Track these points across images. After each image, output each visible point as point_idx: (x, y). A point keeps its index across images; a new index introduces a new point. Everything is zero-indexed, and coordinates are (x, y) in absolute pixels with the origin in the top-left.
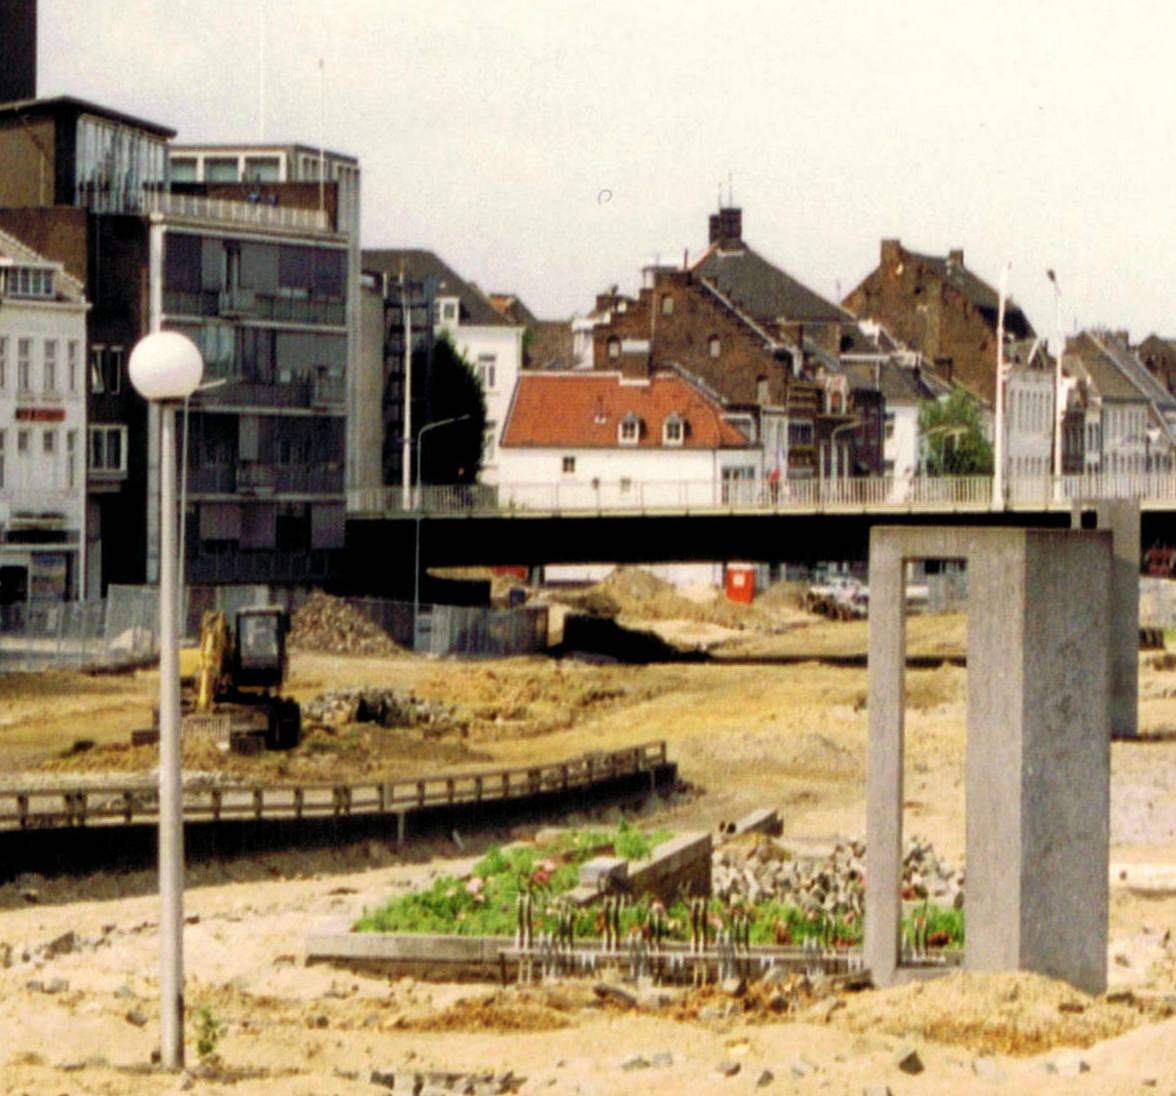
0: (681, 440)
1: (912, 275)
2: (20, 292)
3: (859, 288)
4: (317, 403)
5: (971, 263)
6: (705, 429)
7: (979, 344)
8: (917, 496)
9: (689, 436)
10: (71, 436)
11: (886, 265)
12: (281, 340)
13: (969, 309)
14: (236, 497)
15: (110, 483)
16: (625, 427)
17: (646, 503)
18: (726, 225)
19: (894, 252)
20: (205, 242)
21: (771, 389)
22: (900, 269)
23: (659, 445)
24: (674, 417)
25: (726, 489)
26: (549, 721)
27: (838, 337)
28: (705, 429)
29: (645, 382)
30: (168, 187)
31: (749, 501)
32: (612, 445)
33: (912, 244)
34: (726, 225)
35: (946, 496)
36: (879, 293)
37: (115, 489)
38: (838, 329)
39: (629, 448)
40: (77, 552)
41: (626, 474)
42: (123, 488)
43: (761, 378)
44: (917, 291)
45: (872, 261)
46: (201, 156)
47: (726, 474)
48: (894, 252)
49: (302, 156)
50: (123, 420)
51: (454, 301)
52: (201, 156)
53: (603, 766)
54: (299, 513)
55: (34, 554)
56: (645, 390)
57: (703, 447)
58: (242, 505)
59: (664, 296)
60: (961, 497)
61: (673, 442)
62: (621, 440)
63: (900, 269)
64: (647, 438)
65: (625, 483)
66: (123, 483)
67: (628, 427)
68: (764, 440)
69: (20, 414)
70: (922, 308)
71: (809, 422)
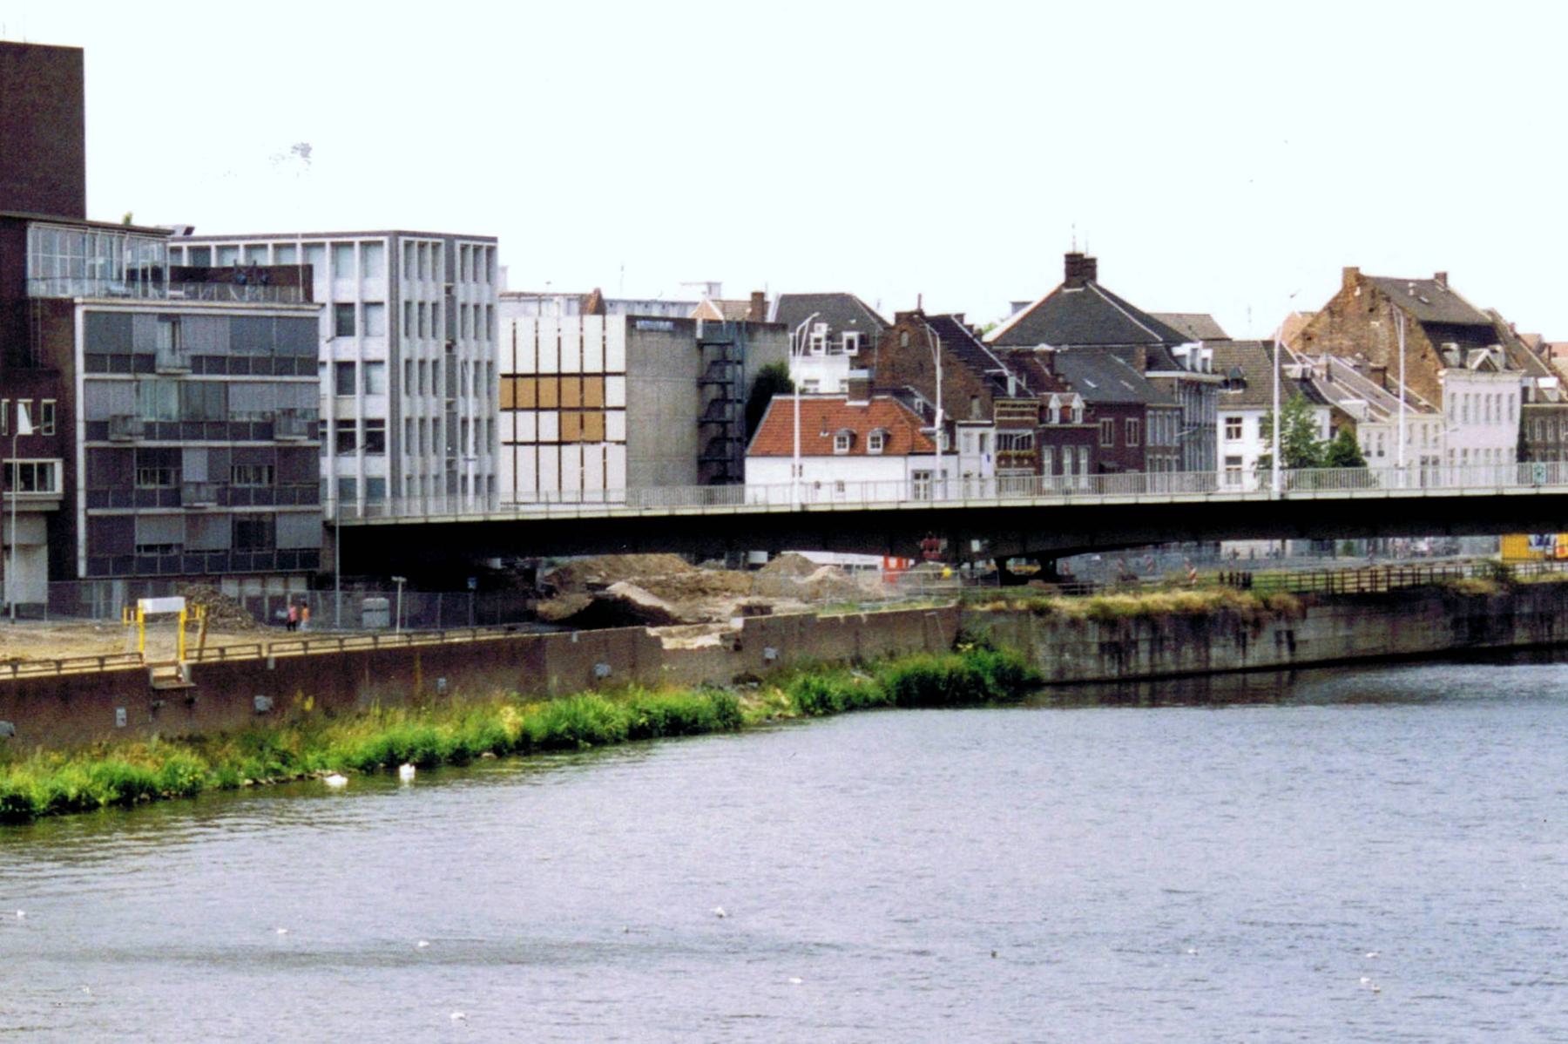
1: (1367, 297)
3: (1325, 309)
5: (1454, 284)
6: (900, 442)
7: (1421, 353)
8: (1291, 484)
9: (889, 445)
11: (1347, 290)
12: (232, 389)
15: (50, 501)
16: (839, 439)
17: (772, 501)
18: (1080, 268)
19: (1354, 278)
20: (135, 320)
21: (982, 405)
22: (1358, 293)
23: (864, 454)
24: (877, 432)
26: (1089, 675)
29: (865, 403)
30: (167, 275)
31: (948, 496)
32: (829, 453)
33: (1367, 271)
34: (1080, 268)
35: (695, 501)
36: (1341, 313)
37: (56, 507)
38: (1144, 351)
41: (841, 478)
43: (974, 397)
44: (1371, 310)
45: (1334, 287)
46: (299, 242)
47: (917, 476)
48: (1354, 278)
50: (56, 455)
51: (854, 335)
52: (242, 243)
54: (266, 519)
56: (864, 410)
57: (898, 454)
58: (188, 516)
59: (902, 331)
60: (711, 500)
61: (876, 451)
62: (837, 450)
63: (1358, 293)
64: (855, 447)
65: (841, 486)
66: (61, 502)
67: (841, 439)
70: (1375, 324)
71: (1030, 432)
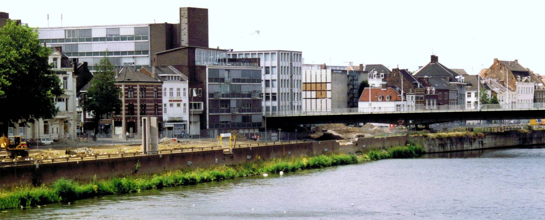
0: (381, 100)
1: (499, 65)
2: (174, 80)
4: (215, 97)
5: (519, 62)
8: (482, 108)
9: (391, 99)
10: (185, 105)
11: (495, 64)
12: (242, 86)
13: (510, 72)
14: (230, 114)
18: (434, 59)
19: (496, 61)
21: (412, 90)
22: (497, 64)
23: (385, 101)
25: (397, 108)
27: (449, 79)
28: (393, 98)
29: (385, 89)
30: (227, 60)
31: (404, 110)
32: (377, 101)
33: (499, 59)
34: (434, 59)
36: (494, 69)
37: (202, 113)
39: (388, 101)
40: (187, 124)
41: (380, 106)
42: (39, 118)
43: (410, 88)
44: (500, 68)
45: (492, 63)
47: (397, 106)
48: (496, 61)
49: (280, 52)
50: (202, 101)
52: (257, 53)
53: (140, 165)
54: (250, 116)
55: (174, 125)
57: (393, 101)
58: (232, 115)
59: (394, 73)
60: (350, 111)
62: (379, 100)
64: (383, 99)
65: (380, 108)
68: (406, 99)
69: (170, 101)
70: (501, 71)
